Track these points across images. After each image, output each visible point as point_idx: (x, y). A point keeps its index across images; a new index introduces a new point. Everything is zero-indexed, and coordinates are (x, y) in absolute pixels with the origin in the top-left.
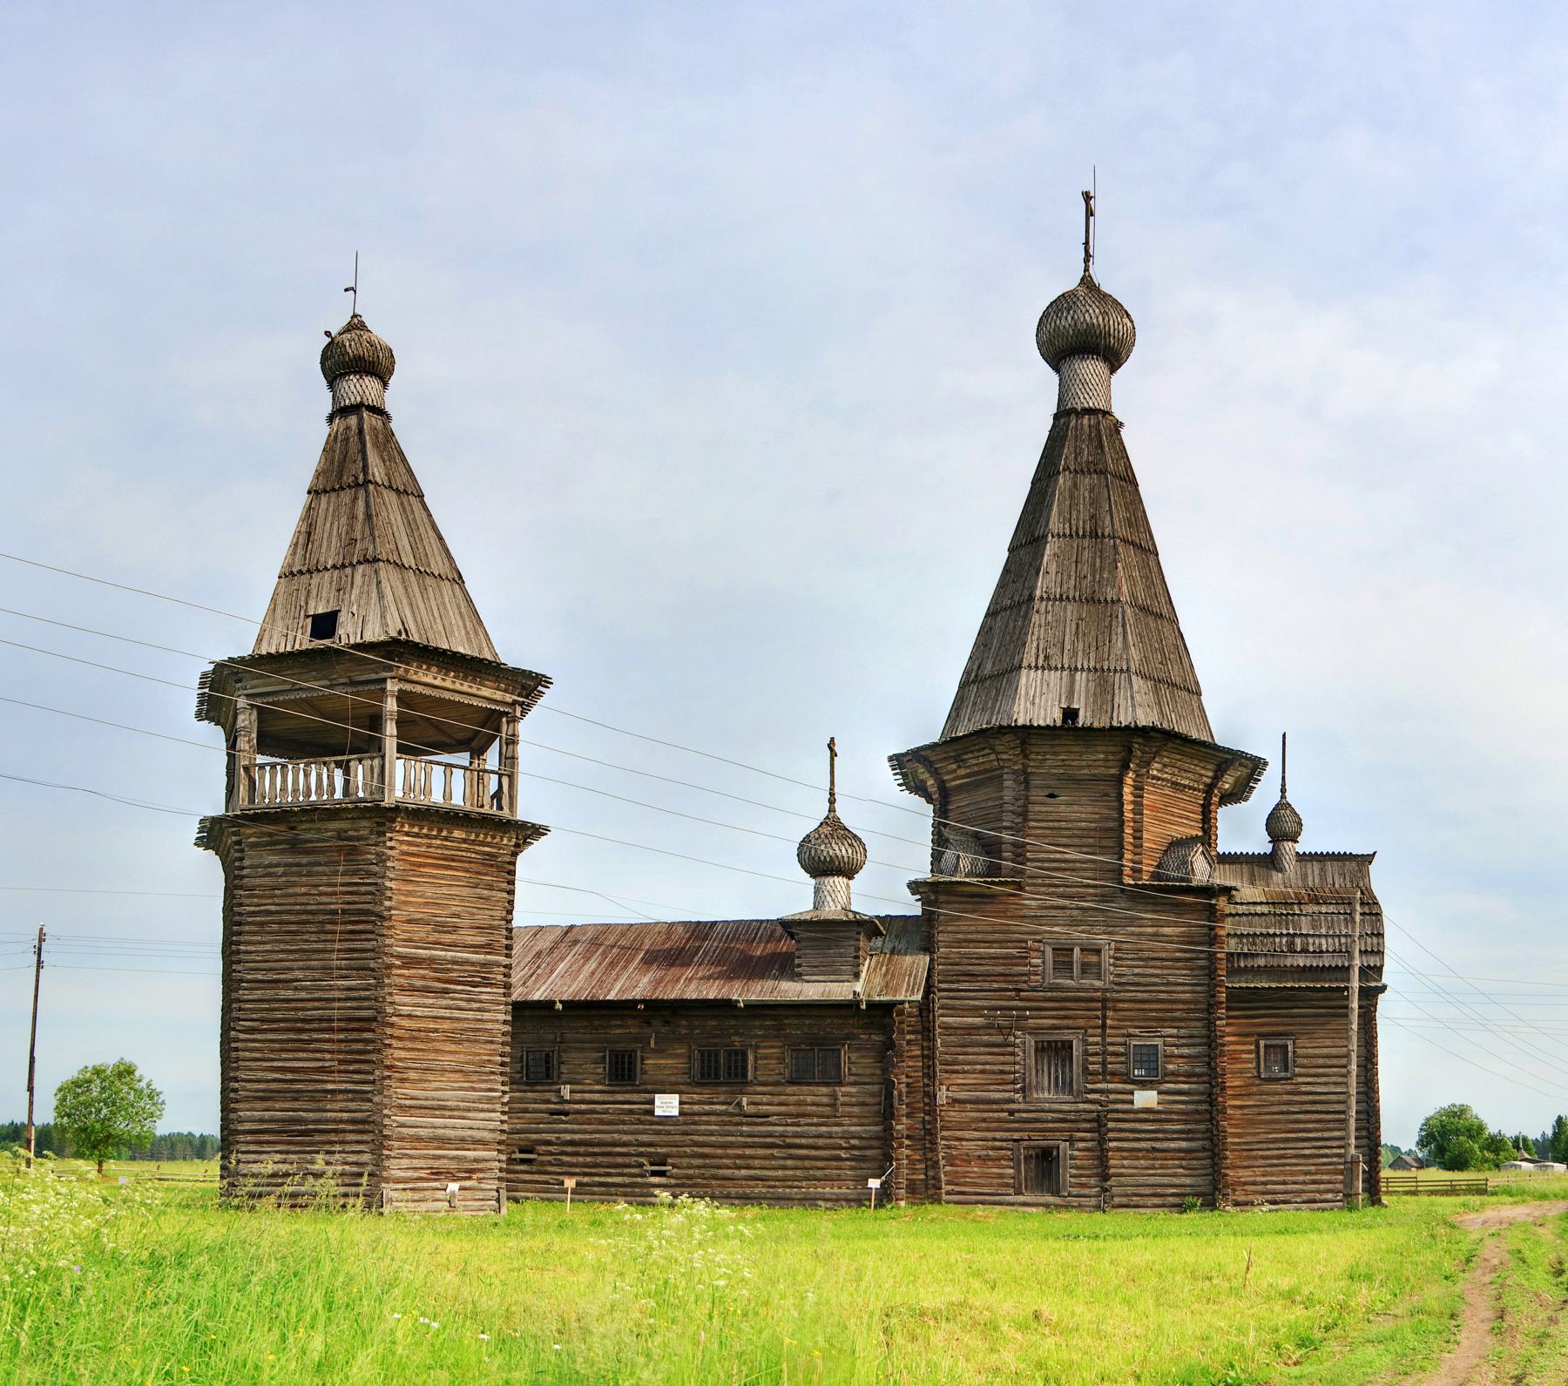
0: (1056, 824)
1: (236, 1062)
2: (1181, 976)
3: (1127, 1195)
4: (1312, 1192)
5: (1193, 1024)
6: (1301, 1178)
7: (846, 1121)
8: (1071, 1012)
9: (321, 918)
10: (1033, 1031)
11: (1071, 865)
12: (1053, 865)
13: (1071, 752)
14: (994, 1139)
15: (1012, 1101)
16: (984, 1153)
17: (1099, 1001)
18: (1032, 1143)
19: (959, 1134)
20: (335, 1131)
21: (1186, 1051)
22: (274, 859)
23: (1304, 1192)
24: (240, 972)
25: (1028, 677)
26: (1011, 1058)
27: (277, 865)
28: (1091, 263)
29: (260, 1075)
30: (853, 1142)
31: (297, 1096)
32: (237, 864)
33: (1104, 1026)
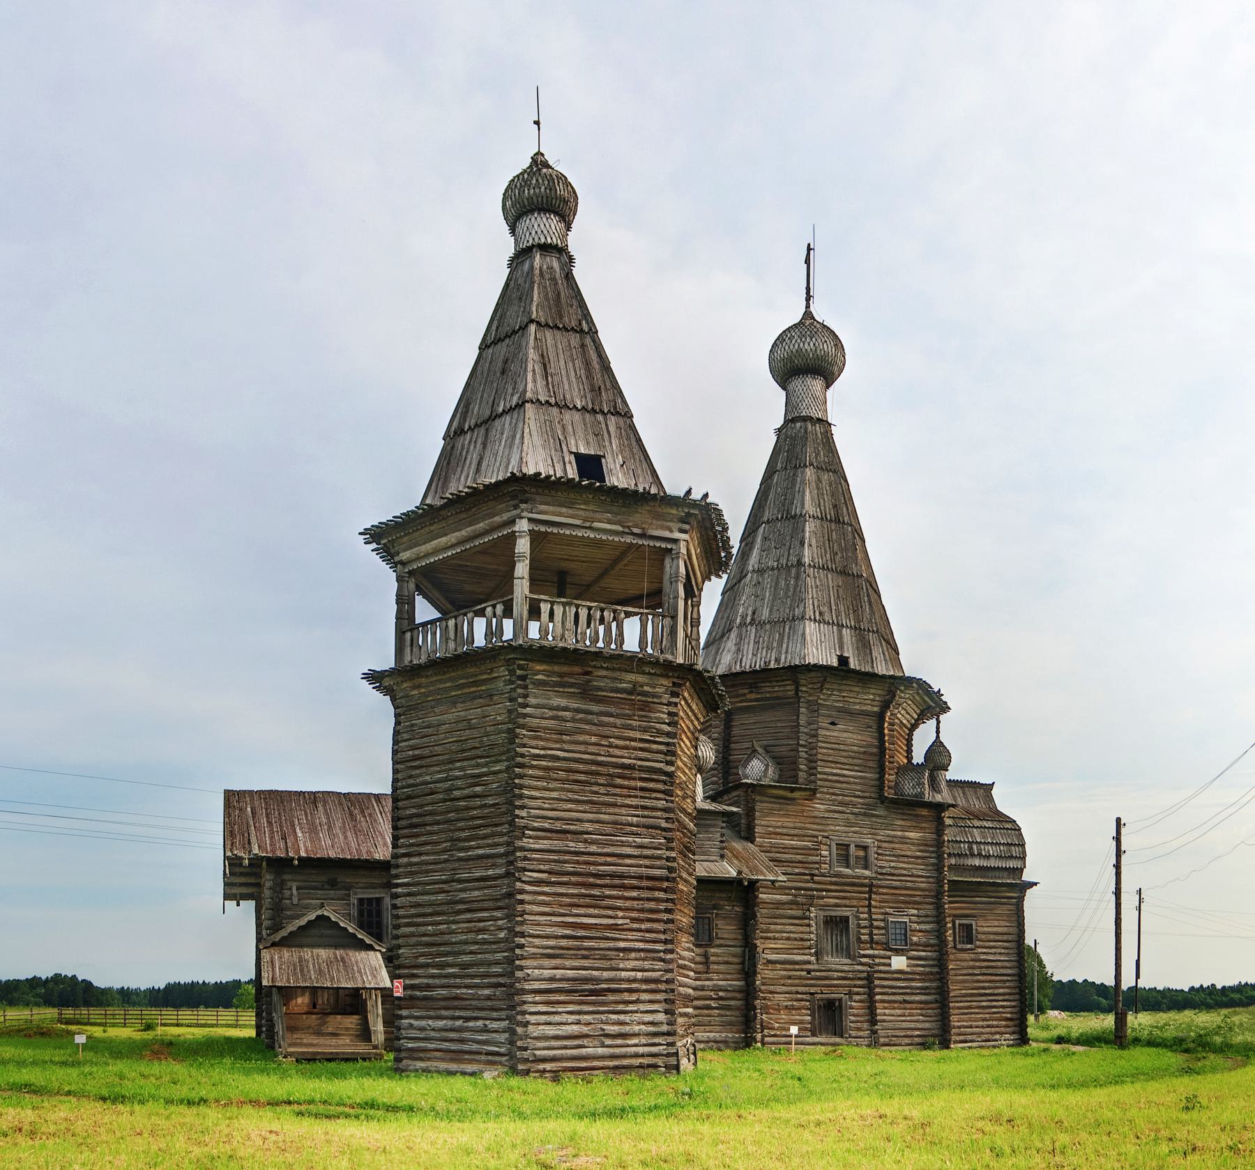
0: (837, 746)
1: (521, 916)
2: (919, 870)
3: (888, 1037)
4: (988, 1033)
5: (928, 906)
6: (981, 1023)
7: (715, 976)
8: (848, 894)
9: (612, 771)
10: (823, 907)
11: (846, 779)
12: (835, 778)
13: (851, 691)
14: (797, 993)
15: (809, 962)
16: (790, 1003)
17: (866, 886)
18: (823, 996)
19: (772, 988)
20: (630, 991)
21: (923, 927)
22: (563, 702)
23: (983, 1033)
24: (523, 818)
25: (810, 628)
26: (808, 929)
27: (566, 709)
28: (811, 302)
29: (549, 930)
30: (721, 994)
31: (588, 954)
32: (520, 700)
33: (870, 906)
